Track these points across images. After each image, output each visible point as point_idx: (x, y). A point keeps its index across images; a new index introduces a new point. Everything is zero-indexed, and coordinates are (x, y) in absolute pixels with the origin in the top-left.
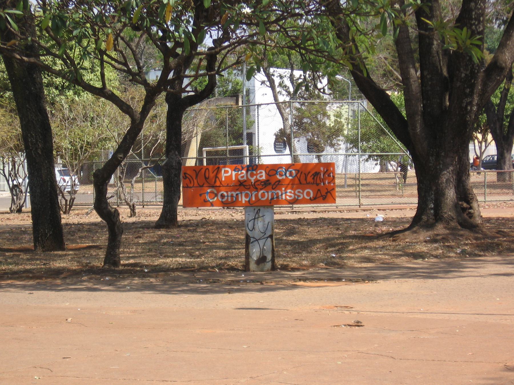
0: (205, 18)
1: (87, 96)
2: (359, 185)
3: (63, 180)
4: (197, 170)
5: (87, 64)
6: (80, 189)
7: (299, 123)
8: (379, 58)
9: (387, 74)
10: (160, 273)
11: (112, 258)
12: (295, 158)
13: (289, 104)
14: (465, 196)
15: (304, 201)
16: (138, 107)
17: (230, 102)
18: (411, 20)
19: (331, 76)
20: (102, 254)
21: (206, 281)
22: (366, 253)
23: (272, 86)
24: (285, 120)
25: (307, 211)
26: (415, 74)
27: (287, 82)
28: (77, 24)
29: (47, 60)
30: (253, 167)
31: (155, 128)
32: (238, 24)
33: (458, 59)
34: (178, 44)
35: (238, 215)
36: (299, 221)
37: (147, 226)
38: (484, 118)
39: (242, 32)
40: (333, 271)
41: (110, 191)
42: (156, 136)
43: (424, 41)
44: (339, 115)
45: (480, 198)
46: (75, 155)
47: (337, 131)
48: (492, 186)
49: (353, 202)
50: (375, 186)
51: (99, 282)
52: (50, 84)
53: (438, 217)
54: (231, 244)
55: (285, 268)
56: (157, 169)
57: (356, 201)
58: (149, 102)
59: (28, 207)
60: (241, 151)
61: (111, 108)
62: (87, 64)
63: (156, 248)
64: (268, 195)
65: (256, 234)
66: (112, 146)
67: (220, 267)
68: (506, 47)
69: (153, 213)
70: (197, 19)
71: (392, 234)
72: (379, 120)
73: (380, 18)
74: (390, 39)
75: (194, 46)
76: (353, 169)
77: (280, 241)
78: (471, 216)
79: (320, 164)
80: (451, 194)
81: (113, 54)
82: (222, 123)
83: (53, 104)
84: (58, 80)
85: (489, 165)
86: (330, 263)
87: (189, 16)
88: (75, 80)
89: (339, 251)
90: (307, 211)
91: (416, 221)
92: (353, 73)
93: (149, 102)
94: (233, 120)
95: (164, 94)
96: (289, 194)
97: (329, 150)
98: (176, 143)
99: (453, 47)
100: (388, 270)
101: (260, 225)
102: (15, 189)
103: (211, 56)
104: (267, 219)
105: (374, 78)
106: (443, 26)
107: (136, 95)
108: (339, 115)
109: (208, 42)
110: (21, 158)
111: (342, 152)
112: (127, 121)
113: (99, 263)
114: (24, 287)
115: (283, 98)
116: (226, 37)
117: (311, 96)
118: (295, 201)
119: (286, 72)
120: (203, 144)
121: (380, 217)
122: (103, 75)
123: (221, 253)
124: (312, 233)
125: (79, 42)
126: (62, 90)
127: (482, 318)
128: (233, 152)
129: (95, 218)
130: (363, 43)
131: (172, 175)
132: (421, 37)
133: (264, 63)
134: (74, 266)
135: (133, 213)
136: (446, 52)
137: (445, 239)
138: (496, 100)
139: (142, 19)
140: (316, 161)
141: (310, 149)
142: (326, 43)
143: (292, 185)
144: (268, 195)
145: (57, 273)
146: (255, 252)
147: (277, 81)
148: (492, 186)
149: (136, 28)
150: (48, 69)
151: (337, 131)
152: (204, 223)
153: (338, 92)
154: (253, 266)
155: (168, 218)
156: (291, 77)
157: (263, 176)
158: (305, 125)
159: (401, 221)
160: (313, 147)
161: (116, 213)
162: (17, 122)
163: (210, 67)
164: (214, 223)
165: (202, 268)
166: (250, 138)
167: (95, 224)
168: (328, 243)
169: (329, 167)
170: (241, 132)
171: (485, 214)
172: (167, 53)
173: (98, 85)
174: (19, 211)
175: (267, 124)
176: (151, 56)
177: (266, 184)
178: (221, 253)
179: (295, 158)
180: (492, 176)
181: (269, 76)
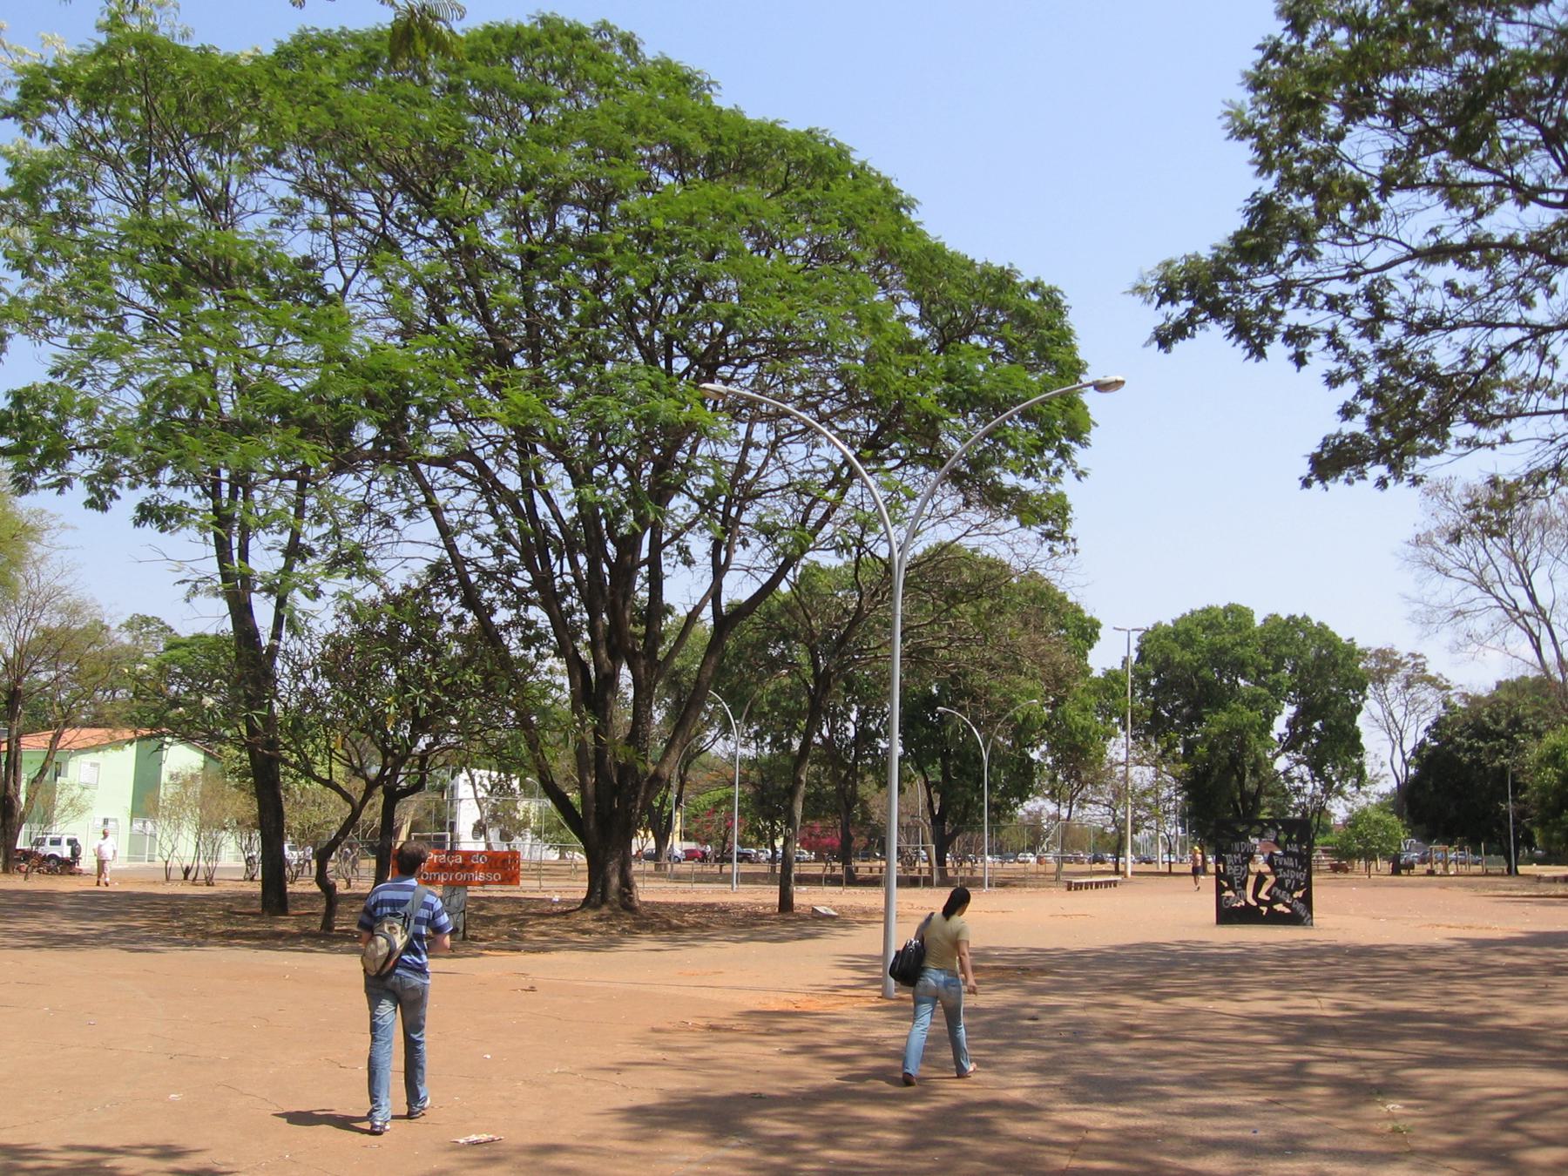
0: (420, 726)
2: (541, 869)
3: (291, 854)
7: (494, 816)
8: (562, 764)
9: (568, 779)
11: (328, 924)
12: (489, 846)
14: (627, 883)
15: (493, 883)
16: (358, 797)
17: (437, 796)
18: (589, 738)
19: (522, 779)
20: (319, 921)
23: (473, 784)
24: (482, 813)
25: (496, 891)
26: (591, 780)
27: (486, 782)
28: (311, 726)
29: (286, 754)
31: (372, 815)
33: (626, 770)
34: (395, 747)
38: (646, 818)
39: (450, 739)
40: (515, 943)
41: (330, 866)
42: (372, 821)
43: (600, 754)
44: (527, 811)
45: (639, 885)
46: (302, 834)
47: (525, 824)
48: (650, 874)
50: (554, 869)
52: (286, 774)
53: (604, 900)
55: (474, 938)
56: (372, 849)
57: (537, 883)
58: (368, 793)
59: (259, 876)
60: (444, 837)
61: (335, 796)
62: (318, 758)
64: (463, 877)
66: (334, 829)
68: (150, 36)
71: (565, 913)
72: (560, 817)
73: (724, 601)
74: (571, 750)
75: (409, 749)
76: (536, 855)
77: (471, 914)
78: (631, 900)
80: (615, 881)
82: (429, 813)
83: (287, 790)
84: (293, 771)
85: (648, 857)
86: (512, 936)
87: (407, 724)
88: (308, 773)
90: (496, 891)
91: (586, 903)
93: (368, 793)
94: (439, 811)
95: (380, 788)
96: (480, 877)
97: (517, 840)
98: (389, 826)
100: (560, 943)
102: (249, 860)
103: (423, 757)
108: (527, 811)
110: (257, 834)
111: (529, 841)
113: (316, 928)
115: (482, 794)
116: (437, 741)
117: (505, 794)
120: (412, 830)
121: (556, 898)
122: (330, 770)
124: (498, 909)
125: (313, 741)
126: (296, 780)
127: (635, 987)
129: (316, 889)
130: (549, 753)
132: (597, 751)
133: (467, 763)
134: (295, 930)
136: (617, 763)
137: (609, 919)
139: (367, 724)
140: (506, 849)
141: (501, 838)
143: (484, 869)
144: (463, 877)
145: (279, 935)
147: (477, 780)
148: (650, 874)
149: (362, 731)
150: (285, 762)
151: (525, 824)
153: (528, 792)
158: (498, 818)
159: (574, 902)
160: (505, 836)
162: (256, 804)
163: (421, 767)
166: (453, 826)
167: (316, 894)
168: (512, 918)
169: (515, 855)
170: (445, 822)
171: (642, 899)
172: (386, 753)
173: (326, 776)
174: (252, 879)
175: (467, 815)
177: (462, 867)
180: (650, 866)
181: (472, 778)
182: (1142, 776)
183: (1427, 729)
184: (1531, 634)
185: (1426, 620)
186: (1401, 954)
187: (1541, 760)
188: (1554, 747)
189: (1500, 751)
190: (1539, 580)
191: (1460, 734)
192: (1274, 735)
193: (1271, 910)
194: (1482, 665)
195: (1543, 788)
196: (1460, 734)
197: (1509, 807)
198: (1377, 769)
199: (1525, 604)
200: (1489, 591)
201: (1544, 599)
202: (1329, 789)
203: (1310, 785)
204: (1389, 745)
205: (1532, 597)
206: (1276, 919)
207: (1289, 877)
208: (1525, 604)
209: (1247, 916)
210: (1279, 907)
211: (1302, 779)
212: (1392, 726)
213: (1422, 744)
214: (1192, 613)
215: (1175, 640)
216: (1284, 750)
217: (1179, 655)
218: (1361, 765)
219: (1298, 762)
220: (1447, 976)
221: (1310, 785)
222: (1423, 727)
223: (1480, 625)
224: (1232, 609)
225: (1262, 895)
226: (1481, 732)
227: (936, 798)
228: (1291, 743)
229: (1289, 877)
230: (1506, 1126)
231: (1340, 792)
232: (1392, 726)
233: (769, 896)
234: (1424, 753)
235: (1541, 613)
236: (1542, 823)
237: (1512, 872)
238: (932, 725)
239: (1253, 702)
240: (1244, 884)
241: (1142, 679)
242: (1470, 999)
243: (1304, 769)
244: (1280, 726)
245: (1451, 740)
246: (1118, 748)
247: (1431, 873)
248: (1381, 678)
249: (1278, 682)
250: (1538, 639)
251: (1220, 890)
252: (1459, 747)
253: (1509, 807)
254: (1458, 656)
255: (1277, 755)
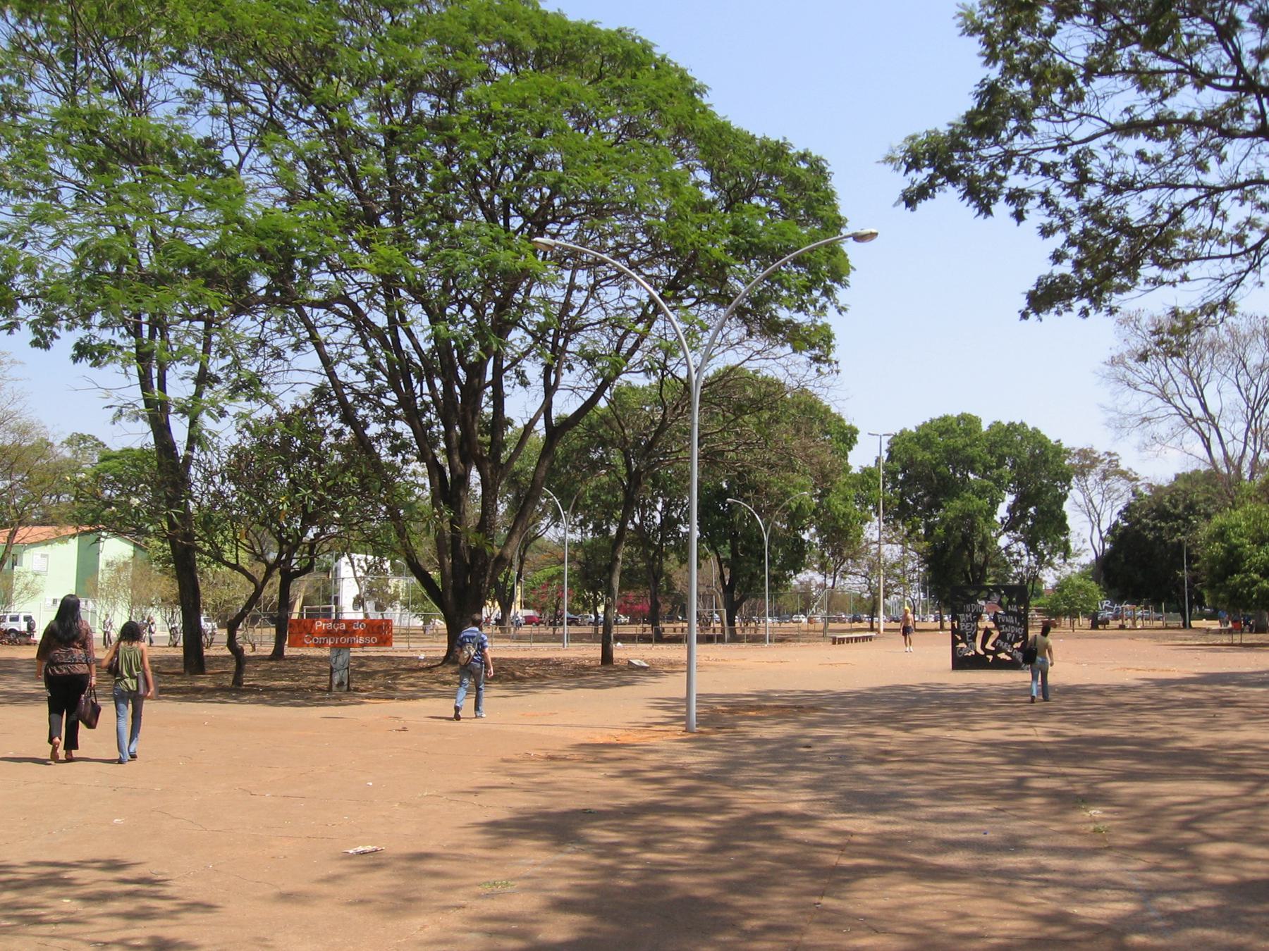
1: (225, 568)
2: (408, 634)
3: (207, 625)
4: (298, 622)
5: (227, 547)
6: (218, 631)
7: (370, 591)
8: (425, 548)
9: (430, 560)
10: (628, 884)
11: (238, 680)
12: (366, 615)
13: (363, 578)
16: (260, 578)
17: (324, 576)
18: (447, 527)
20: (231, 678)
21: (302, 698)
22: (412, 680)
23: (353, 566)
24: (360, 589)
25: (373, 651)
27: (363, 563)
30: (337, 621)
31: (271, 592)
32: (331, 524)
33: (477, 553)
34: (289, 536)
35: (326, 652)
36: (367, 658)
37: (263, 658)
38: (493, 591)
39: (333, 530)
40: (389, 693)
41: (239, 633)
43: (455, 540)
44: (397, 587)
46: (215, 608)
47: (395, 597)
48: (497, 636)
49: (404, 645)
50: (418, 633)
51: (228, 697)
52: (201, 560)
54: (320, 672)
55: (356, 690)
56: (272, 620)
58: (268, 574)
59: (181, 643)
60: (330, 609)
62: (227, 547)
63: (268, 674)
64: (347, 640)
65: (337, 666)
66: (241, 603)
67: (311, 688)
69: (268, 649)
70: (303, 520)
71: (429, 668)
72: (424, 591)
76: (405, 623)
77: (354, 671)
79: (383, 620)
81: (245, 541)
84: (206, 558)
86: (387, 687)
88: (218, 558)
89: (394, 679)
90: (373, 651)
92: (407, 560)
93: (268, 574)
94: (325, 589)
96: (360, 640)
98: (285, 602)
99: (473, 545)
101: (340, 660)
102: (172, 630)
103: (312, 545)
104: (346, 656)
105: (421, 563)
106: (467, 530)
107: (259, 570)
108: (397, 587)
109: (311, 534)
110: (178, 609)
112: (252, 587)
113: (228, 684)
114: (175, 699)
115: (360, 574)
116: (323, 532)
117: (379, 573)
118: (363, 645)
119: (362, 556)
123: (313, 679)
124: (375, 666)
128: (324, 609)
129: (227, 652)
131: (282, 625)
132: (453, 538)
133: (348, 549)
134: (211, 686)
135: (254, 649)
138: (501, 580)
139: (266, 518)
141: (376, 609)
142: (389, 539)
144: (347, 640)
145: (198, 690)
146: (336, 679)
147: (356, 563)
149: (262, 524)
150: (200, 550)
151: (395, 597)
152: (302, 658)
153: (397, 571)
154: (334, 688)
155: (278, 654)
156: (366, 560)
157: (344, 627)
158: (374, 593)
159: (436, 659)
160: (379, 607)
161: (242, 650)
162: (177, 585)
163: (311, 552)
164: (309, 657)
165: (299, 689)
166: (337, 600)
168: (387, 673)
170: (330, 595)
172: (282, 542)
173: (234, 562)
174: (175, 646)
175: (348, 591)
176: (271, 542)
177: (345, 632)
178: (313, 679)
179: (366, 615)
182: (892, 552)
183: (1120, 513)
184: (1203, 436)
185: (1120, 425)
186: (1099, 692)
187: (1210, 537)
188: (1221, 526)
189: (1178, 530)
190: (1209, 392)
191: (1146, 516)
192: (997, 518)
193: (995, 658)
194: (1164, 460)
195: (1212, 559)
196: (1146, 516)
197: (1184, 574)
198: (1080, 545)
199: (1198, 412)
200: (1169, 402)
201: (1213, 408)
202: (1041, 561)
203: (1026, 558)
204: (1089, 525)
205: (1204, 406)
206: (999, 665)
207: (1010, 632)
208: (1198, 412)
209: (977, 663)
210: (1002, 656)
211: (1019, 554)
212: (1092, 510)
213: (1116, 524)
214: (932, 421)
215: (917, 443)
216: (1006, 530)
217: (922, 455)
218: (1067, 542)
219: (1016, 540)
220: (1136, 709)
221: (1026, 558)
222: (1116, 511)
223: (1162, 429)
224: (964, 418)
225: (989, 646)
226: (1163, 514)
227: (727, 571)
228: (1011, 525)
229: (1010, 632)
230: (1185, 826)
231: (1050, 564)
232: (1092, 510)
233: (593, 652)
234: (1118, 532)
235: (1211, 419)
236: (1211, 587)
237: (1186, 626)
238: (722, 513)
239: (981, 492)
240: (974, 638)
241: (892, 474)
242: (1155, 727)
243: (1021, 545)
244: (1002, 512)
245: (1139, 521)
246: (872, 530)
247: (1122, 627)
248: (1082, 472)
249: (1001, 477)
250: (1208, 440)
251: (955, 642)
252: (1145, 527)
253: (1184, 574)
254: (1145, 454)
255: (1001, 534)
